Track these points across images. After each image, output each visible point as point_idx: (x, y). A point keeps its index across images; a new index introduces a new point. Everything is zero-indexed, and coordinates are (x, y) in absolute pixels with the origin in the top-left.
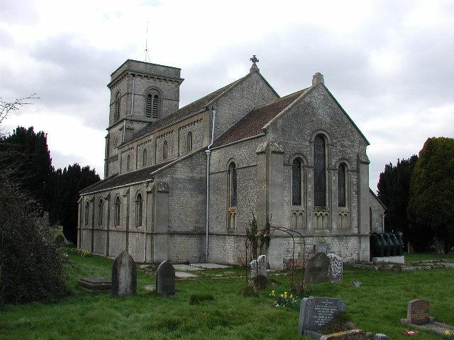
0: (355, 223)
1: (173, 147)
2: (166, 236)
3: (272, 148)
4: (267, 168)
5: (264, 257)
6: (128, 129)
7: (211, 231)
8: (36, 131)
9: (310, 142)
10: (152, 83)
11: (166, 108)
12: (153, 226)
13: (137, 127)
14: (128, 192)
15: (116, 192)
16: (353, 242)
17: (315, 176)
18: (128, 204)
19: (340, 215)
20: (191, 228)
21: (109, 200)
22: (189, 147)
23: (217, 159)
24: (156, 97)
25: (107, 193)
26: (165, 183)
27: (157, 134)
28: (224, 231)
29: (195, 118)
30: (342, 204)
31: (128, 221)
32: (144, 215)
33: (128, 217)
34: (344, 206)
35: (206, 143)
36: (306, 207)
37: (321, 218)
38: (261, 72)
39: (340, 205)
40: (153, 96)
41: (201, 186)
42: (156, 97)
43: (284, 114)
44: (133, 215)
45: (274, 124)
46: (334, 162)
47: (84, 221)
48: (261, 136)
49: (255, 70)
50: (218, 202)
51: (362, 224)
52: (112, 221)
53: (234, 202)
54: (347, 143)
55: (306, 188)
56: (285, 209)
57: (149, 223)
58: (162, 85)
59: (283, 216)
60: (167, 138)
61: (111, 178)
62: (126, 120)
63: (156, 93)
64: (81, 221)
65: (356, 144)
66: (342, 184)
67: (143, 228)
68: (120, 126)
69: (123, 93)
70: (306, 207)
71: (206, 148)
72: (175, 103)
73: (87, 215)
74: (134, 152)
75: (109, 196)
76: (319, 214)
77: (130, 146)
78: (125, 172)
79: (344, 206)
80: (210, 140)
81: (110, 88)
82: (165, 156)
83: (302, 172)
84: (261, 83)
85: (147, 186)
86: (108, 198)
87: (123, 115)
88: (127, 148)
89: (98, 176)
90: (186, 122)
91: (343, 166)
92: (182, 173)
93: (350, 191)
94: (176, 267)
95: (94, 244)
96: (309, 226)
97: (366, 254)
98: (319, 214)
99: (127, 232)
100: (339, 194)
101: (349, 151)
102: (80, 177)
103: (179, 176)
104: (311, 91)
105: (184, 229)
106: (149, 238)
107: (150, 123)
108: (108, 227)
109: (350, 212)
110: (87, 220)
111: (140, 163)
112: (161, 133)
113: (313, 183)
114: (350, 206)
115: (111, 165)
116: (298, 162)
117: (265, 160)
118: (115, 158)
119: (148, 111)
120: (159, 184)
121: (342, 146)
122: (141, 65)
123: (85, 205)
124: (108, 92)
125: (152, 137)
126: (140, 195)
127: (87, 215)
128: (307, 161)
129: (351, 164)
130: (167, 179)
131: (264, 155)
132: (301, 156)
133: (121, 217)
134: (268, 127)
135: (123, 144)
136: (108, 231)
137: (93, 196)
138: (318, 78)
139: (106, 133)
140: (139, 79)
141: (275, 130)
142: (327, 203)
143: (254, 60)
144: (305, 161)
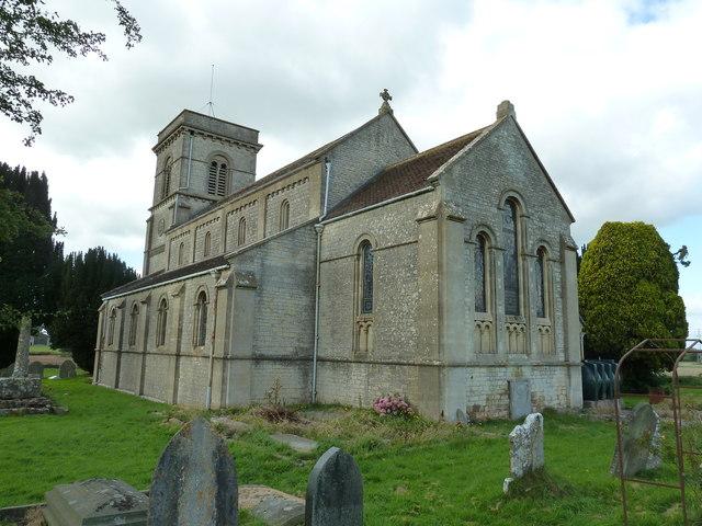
0: (560, 345)
1: (255, 226)
2: (248, 363)
3: (447, 212)
4: (440, 243)
6: (182, 207)
7: (322, 355)
8: (29, 172)
10: (217, 146)
11: (236, 181)
12: (226, 346)
13: (196, 205)
14: (183, 290)
18: (182, 310)
20: (288, 351)
21: (149, 305)
23: (340, 235)
24: (224, 166)
25: (147, 294)
26: (249, 273)
31: (179, 336)
32: (210, 326)
33: (180, 331)
35: (314, 213)
37: (514, 335)
38: (396, 115)
39: (538, 315)
40: (219, 165)
41: (309, 282)
42: (224, 166)
43: (462, 158)
44: (189, 327)
45: (448, 170)
46: (532, 245)
47: (107, 339)
48: (428, 191)
49: (387, 112)
50: (339, 303)
51: (571, 350)
52: (153, 338)
53: (367, 305)
54: (546, 216)
57: (220, 340)
58: (233, 152)
59: (462, 336)
60: (245, 212)
61: (151, 276)
62: (180, 194)
63: (223, 161)
64: (102, 342)
67: (207, 349)
68: (170, 203)
69: (175, 156)
71: (317, 221)
73: (112, 329)
74: (189, 238)
75: (149, 298)
76: (512, 327)
77: (185, 229)
80: (322, 208)
85: (218, 278)
86: (147, 301)
87: (174, 188)
88: (179, 232)
91: (541, 251)
92: (278, 258)
95: (139, 384)
96: (501, 347)
97: (577, 395)
99: (178, 355)
101: (548, 229)
102: (102, 272)
103: (273, 263)
104: (495, 129)
105: (282, 352)
106: (218, 365)
107: (214, 201)
108: (145, 347)
110: (111, 338)
112: (237, 205)
114: (552, 317)
115: (154, 259)
116: (482, 238)
117: (435, 232)
118: (161, 249)
119: (211, 185)
120: (238, 274)
121: (541, 220)
122: (203, 120)
123: (110, 314)
124: (154, 157)
125: (219, 213)
126: (203, 295)
127: (112, 329)
130: (254, 267)
131: (433, 223)
132: (486, 230)
133: (168, 331)
134: (441, 174)
135: (173, 227)
136: (144, 354)
137: (123, 299)
138: (506, 112)
139: (149, 215)
140: (199, 138)
141: (451, 183)
143: (386, 96)
144: (492, 238)
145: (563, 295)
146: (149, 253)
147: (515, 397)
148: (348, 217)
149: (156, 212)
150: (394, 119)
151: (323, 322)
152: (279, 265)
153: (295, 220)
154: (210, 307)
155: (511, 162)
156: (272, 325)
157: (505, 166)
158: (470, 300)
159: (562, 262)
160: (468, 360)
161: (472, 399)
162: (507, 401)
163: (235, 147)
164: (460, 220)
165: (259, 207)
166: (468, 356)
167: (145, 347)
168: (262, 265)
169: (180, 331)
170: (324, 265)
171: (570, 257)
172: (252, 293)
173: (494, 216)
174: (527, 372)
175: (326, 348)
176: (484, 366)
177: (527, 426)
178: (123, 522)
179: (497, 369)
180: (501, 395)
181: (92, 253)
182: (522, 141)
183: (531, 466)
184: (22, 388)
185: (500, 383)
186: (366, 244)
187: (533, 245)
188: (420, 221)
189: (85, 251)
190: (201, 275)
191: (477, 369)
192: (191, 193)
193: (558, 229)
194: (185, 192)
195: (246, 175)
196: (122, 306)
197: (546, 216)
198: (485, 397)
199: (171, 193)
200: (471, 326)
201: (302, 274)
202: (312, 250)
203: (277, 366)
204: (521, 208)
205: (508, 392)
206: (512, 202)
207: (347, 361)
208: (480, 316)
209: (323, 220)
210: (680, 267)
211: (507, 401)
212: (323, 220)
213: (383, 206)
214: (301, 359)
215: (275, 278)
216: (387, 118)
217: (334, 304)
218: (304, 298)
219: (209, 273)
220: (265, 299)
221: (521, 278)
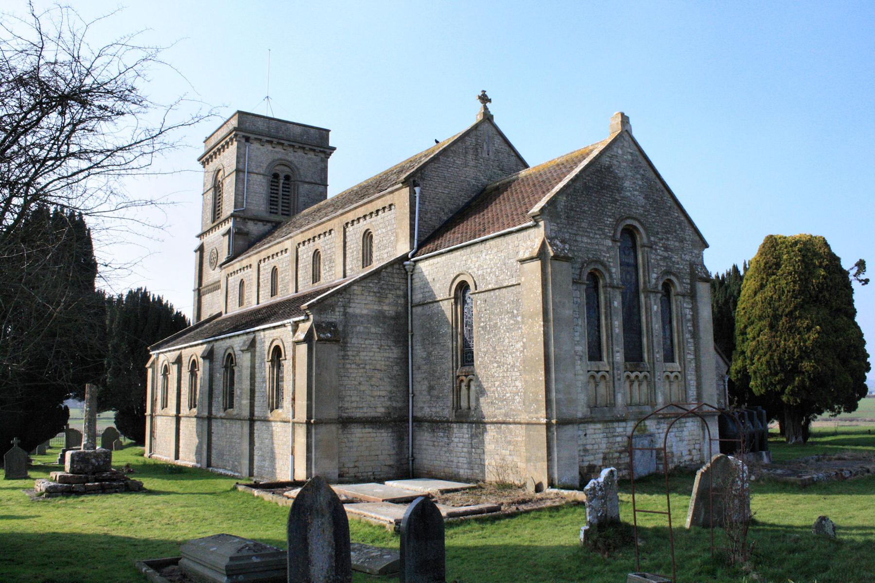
2: (334, 428)
5: (612, 472)
7: (419, 414)
9: (614, 241)
10: (279, 153)
15: (228, 342)
16: (691, 426)
17: (623, 303)
19: (668, 377)
22: (367, 258)
24: (287, 178)
26: (331, 324)
27: (300, 238)
28: (447, 413)
29: (379, 204)
30: (669, 357)
32: (287, 386)
33: (252, 392)
34: (673, 361)
35: (403, 248)
36: (612, 364)
37: (636, 384)
38: (496, 121)
40: (282, 176)
42: (287, 178)
49: (488, 117)
54: (673, 243)
55: (610, 328)
56: (578, 367)
60: (319, 244)
65: (687, 245)
66: (667, 320)
70: (612, 364)
71: (405, 258)
72: (321, 188)
78: (234, 310)
79: (673, 361)
81: (203, 163)
82: (316, 278)
83: (602, 297)
84: (498, 140)
85: (295, 331)
89: (178, 314)
90: (360, 212)
91: (667, 286)
93: (681, 333)
94: (342, 490)
96: (619, 398)
97: (658, 446)
98: (633, 375)
100: (664, 338)
101: (676, 258)
103: (358, 311)
105: (371, 413)
109: (683, 373)
111: (266, 290)
112: (309, 235)
113: (621, 318)
116: (594, 277)
117: (539, 274)
118: (215, 286)
119: (272, 202)
121: (666, 249)
125: (288, 244)
128: (611, 277)
129: (681, 283)
132: (600, 267)
133: (237, 392)
137: (178, 352)
139: (197, 243)
140: (256, 145)
142: (646, 356)
143: (484, 99)
144: (607, 276)
145: (695, 335)
146: (199, 294)
147: (638, 454)
148: (442, 254)
149: (207, 239)
150: (495, 127)
151: (419, 376)
152: (365, 312)
153: (381, 258)
154: (287, 365)
155: (627, 184)
156: (360, 384)
157: (620, 189)
158: (582, 348)
159: (692, 295)
160: (580, 415)
161: (586, 458)
162: (628, 460)
163: (300, 153)
164: (566, 259)
165: (336, 238)
166: (581, 411)
167: (652, 452)
168: (345, 314)
169: (252, 392)
170: (418, 310)
171: (704, 290)
172: (336, 347)
173: (609, 249)
174: (651, 425)
175: (424, 407)
176: (599, 422)
177: (601, 479)
178: (258, 560)
179: (616, 424)
180: (621, 452)
181: (132, 295)
182: (640, 159)
183: (606, 515)
184: (93, 461)
185: (619, 439)
186: (463, 287)
187: (657, 279)
188: (522, 261)
189: (125, 293)
190: (274, 327)
191: (592, 426)
192: (249, 215)
193: (688, 257)
194: (241, 214)
195: (316, 187)
196: (179, 361)
197: (673, 243)
198: (601, 456)
199: (223, 217)
200: (583, 378)
201: (393, 322)
202: (400, 293)
203: (367, 430)
204: (641, 238)
205: (629, 449)
206: (630, 232)
207: (448, 422)
208: (594, 365)
209: (413, 256)
210: (855, 285)
211: (628, 460)
212: (413, 256)
213: (482, 241)
214: (395, 421)
215: (359, 328)
216: (486, 125)
217: (429, 354)
218: (395, 350)
219: (284, 325)
220: (350, 353)
221: (644, 319)
